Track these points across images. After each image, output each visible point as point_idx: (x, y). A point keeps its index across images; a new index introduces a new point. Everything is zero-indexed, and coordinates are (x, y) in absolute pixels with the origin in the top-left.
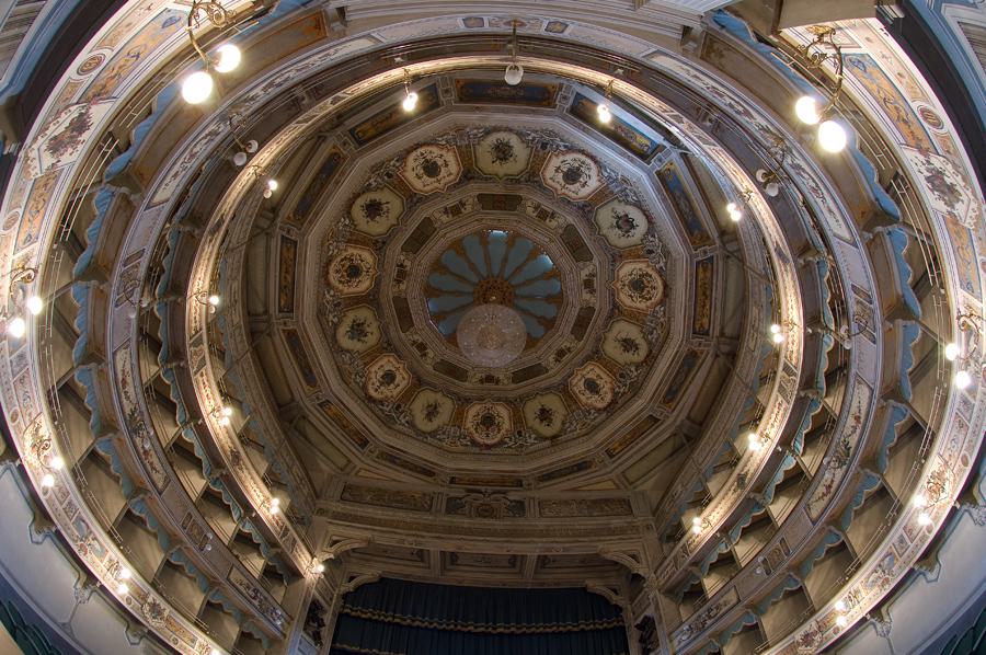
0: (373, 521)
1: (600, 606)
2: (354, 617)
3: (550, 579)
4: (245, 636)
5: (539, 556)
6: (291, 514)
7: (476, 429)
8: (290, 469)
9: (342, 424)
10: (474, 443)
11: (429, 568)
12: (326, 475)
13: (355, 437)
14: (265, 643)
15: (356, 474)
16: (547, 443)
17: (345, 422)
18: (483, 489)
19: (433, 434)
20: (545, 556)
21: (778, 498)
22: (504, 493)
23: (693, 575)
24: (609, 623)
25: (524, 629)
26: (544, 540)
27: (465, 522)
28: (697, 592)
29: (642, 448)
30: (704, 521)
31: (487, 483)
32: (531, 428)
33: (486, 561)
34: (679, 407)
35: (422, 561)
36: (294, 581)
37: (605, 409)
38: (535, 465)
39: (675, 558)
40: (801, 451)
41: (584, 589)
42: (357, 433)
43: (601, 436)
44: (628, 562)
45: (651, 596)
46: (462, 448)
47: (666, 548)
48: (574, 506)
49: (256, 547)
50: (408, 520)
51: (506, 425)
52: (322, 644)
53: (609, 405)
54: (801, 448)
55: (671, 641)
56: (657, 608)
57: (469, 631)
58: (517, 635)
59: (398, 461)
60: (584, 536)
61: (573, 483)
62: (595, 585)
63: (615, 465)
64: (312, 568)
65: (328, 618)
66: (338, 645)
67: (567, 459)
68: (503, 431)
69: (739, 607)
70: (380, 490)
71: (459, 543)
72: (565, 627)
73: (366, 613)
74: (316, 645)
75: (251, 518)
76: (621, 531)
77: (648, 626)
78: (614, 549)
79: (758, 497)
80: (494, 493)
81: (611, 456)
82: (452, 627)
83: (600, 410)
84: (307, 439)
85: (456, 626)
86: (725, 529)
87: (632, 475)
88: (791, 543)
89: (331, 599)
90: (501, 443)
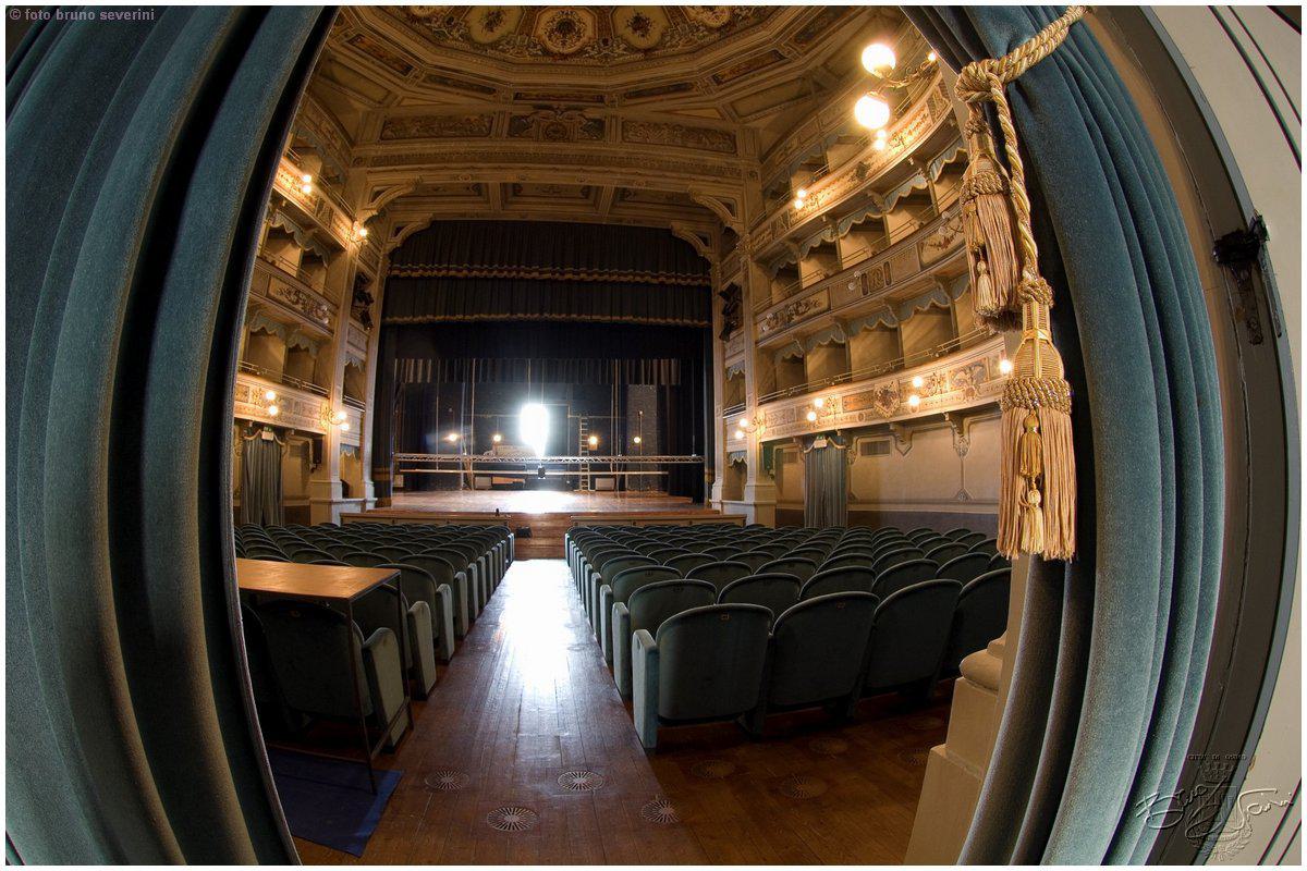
0: (422, 159)
1: (682, 254)
2: (403, 279)
3: (629, 215)
4: (293, 352)
5: (617, 188)
6: (326, 181)
7: (550, 37)
8: (318, 128)
9: (378, 54)
10: (546, 52)
11: (488, 202)
12: (361, 114)
13: (396, 66)
14: (313, 351)
15: (398, 105)
16: (640, 56)
17: (381, 53)
18: (555, 104)
19: (494, 45)
20: (625, 189)
21: (900, 211)
22: (581, 110)
23: (790, 252)
24: (693, 279)
25: (596, 276)
26: (623, 170)
27: (530, 146)
28: (791, 273)
29: (758, 83)
30: (811, 196)
31: (560, 98)
32: (621, 37)
33: (553, 192)
34: (815, 52)
35: (480, 195)
36: (334, 259)
37: (718, 29)
38: (621, 79)
40: (936, 179)
41: (669, 231)
42: (397, 60)
43: (708, 59)
44: (723, 211)
45: (742, 260)
46: (532, 59)
47: (769, 205)
48: (665, 132)
49: (290, 238)
50: (462, 150)
51: (589, 32)
52: (371, 326)
53: (725, 26)
54: (937, 175)
55: (756, 324)
56: (746, 277)
57: (533, 278)
58: (587, 283)
59: (449, 82)
60: (672, 171)
61: (667, 105)
62: (683, 229)
63: (721, 94)
64: (353, 234)
65: (375, 290)
66: (388, 319)
67: (662, 78)
68: (585, 39)
69: (827, 317)
70: (427, 117)
71: (522, 173)
72: (642, 276)
73: (417, 270)
74: (366, 329)
75: (281, 208)
76: (720, 172)
77: (733, 295)
78: (707, 193)
79: (877, 199)
80: (568, 109)
81: (719, 83)
82: (514, 274)
83: (711, 28)
84: (337, 82)
85: (518, 272)
86: (834, 216)
87: (743, 108)
88: (895, 273)
89: (377, 263)
90: (581, 52)
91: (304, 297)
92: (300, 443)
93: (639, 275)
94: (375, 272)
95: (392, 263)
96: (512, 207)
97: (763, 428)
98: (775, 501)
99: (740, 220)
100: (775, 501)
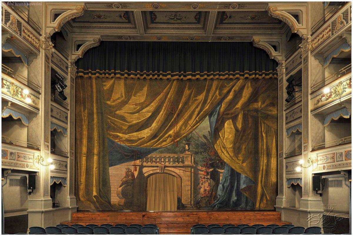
5: (219, 12)
11: (135, 28)
24: (266, 75)
35: (129, 22)
39: (334, 23)
41: (251, 44)
62: (261, 40)
72: (234, 75)
77: (296, 81)
89: (67, 68)
91: (8, 83)
92: (19, 178)
93: (232, 74)
94: (67, 74)
95: (78, 69)
96: (152, 31)
97: (315, 165)
98: (323, 210)
99: (304, 26)
100: (323, 210)
